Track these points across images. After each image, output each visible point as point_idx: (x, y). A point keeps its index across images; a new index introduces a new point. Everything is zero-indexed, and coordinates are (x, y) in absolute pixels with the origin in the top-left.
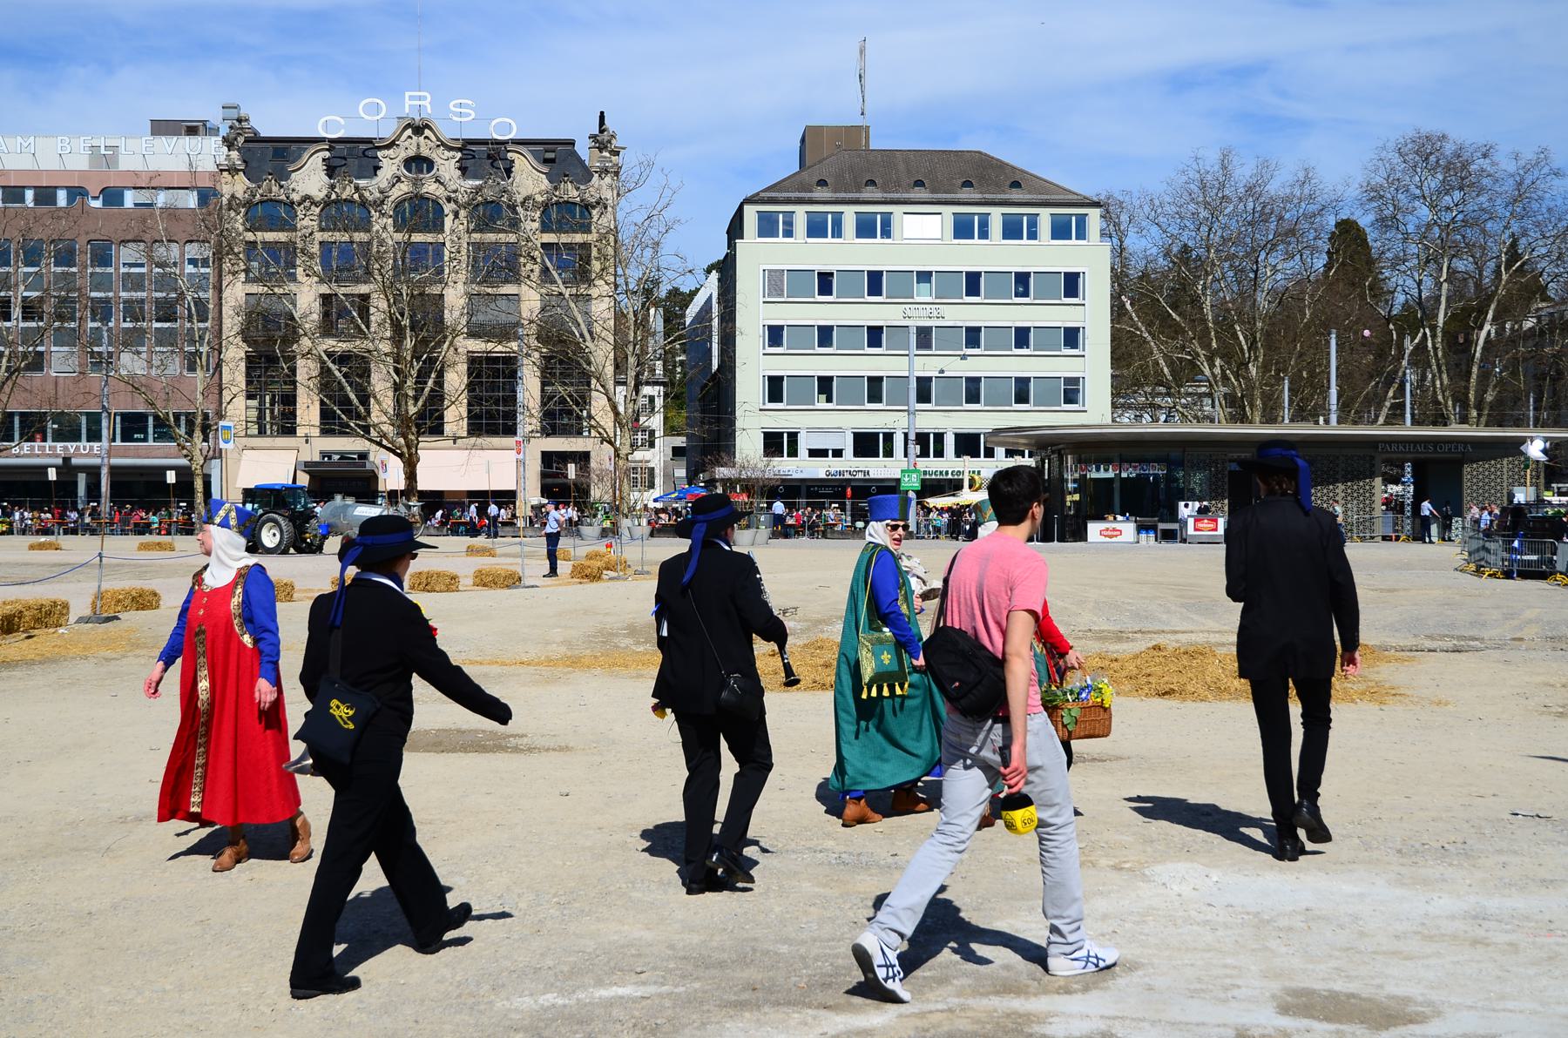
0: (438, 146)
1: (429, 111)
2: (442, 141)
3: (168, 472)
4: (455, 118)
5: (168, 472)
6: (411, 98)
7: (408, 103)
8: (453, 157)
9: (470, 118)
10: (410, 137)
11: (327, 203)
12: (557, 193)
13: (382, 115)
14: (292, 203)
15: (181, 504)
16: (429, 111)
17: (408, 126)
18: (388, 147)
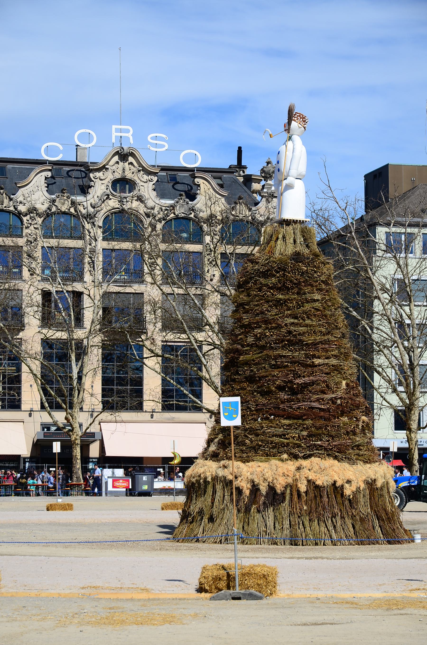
0: (139, 171)
1: (132, 141)
2: (143, 167)
3: (54, 443)
4: (152, 149)
5: (54, 443)
6: (117, 130)
7: (114, 134)
8: (151, 180)
9: (164, 149)
10: (117, 163)
11: (48, 215)
12: (233, 213)
13: (93, 143)
14: (20, 213)
15: (51, 469)
16: (132, 141)
17: (117, 153)
18: (99, 170)
